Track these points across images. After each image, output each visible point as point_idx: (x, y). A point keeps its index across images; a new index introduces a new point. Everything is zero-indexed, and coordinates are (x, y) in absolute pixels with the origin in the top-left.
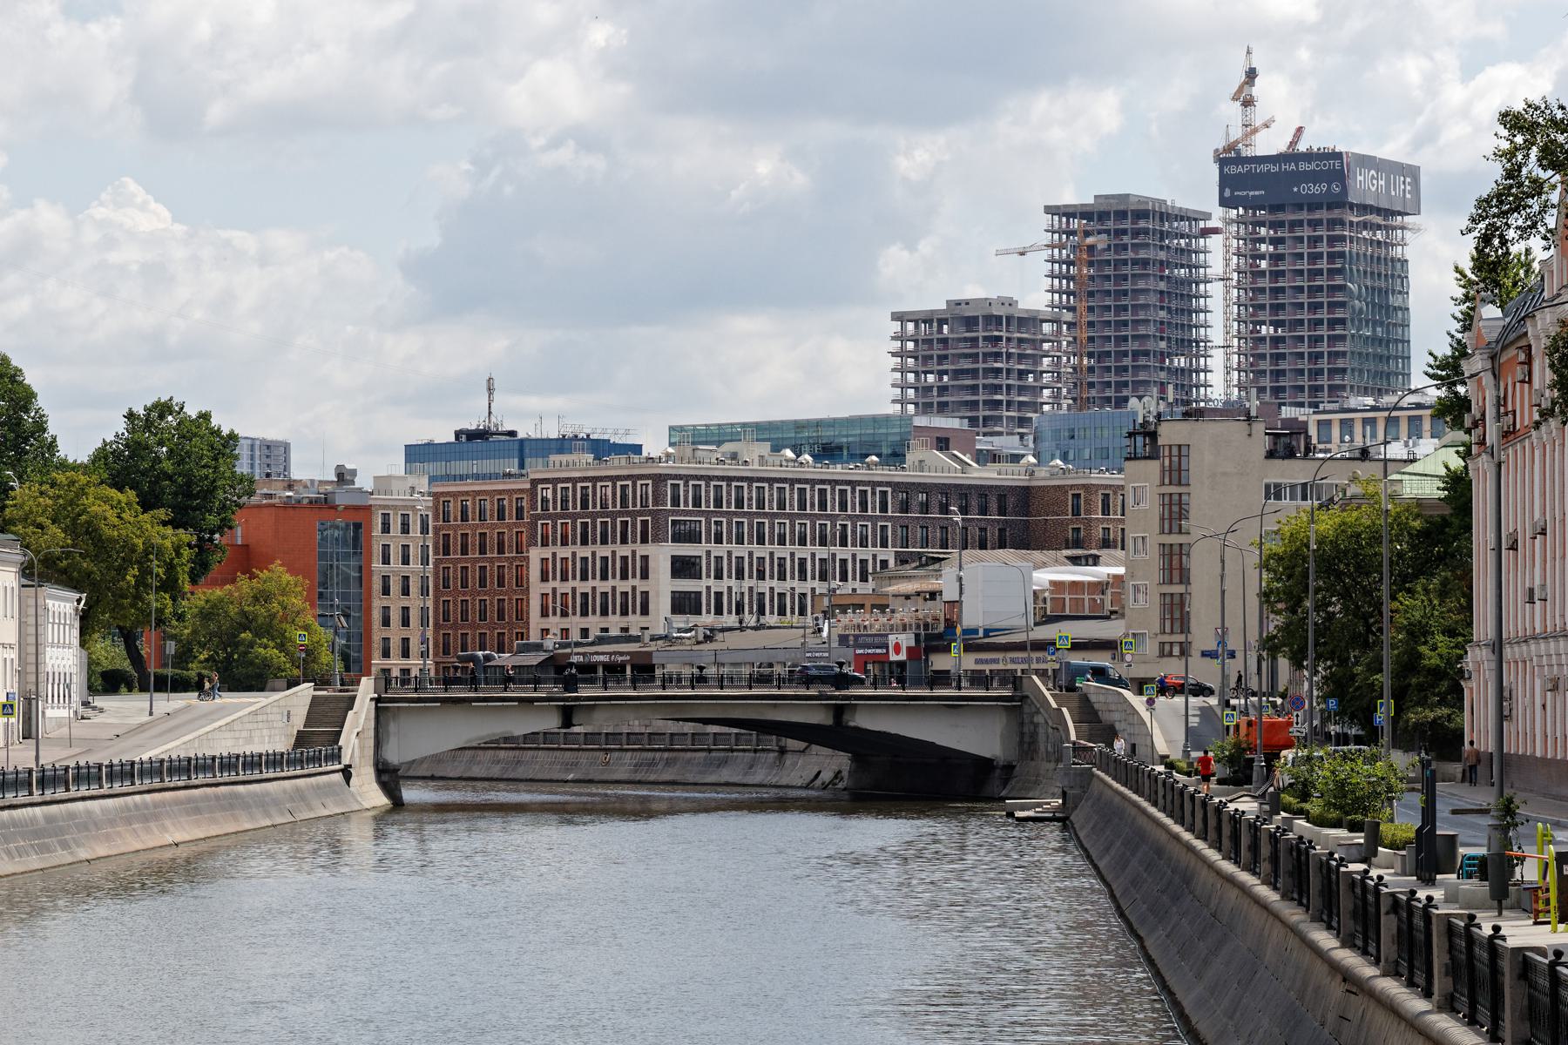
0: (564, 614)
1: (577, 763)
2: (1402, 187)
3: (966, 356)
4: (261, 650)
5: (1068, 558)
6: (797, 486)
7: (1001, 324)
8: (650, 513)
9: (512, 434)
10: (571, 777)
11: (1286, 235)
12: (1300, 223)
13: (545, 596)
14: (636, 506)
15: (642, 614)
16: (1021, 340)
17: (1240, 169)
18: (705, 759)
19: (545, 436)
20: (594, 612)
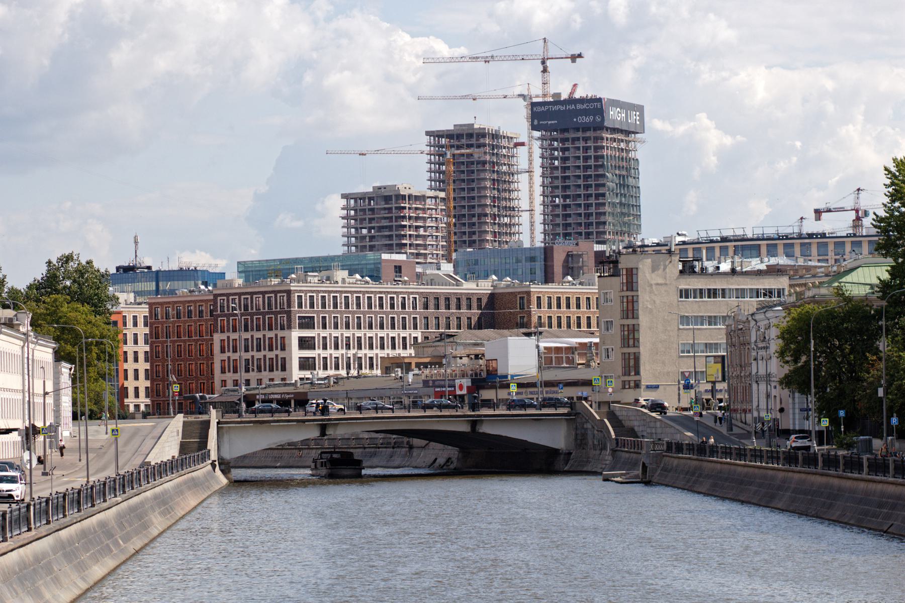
0: (235, 371)
1: (282, 457)
2: (634, 117)
3: (385, 218)
5: (523, 333)
6: (367, 295)
7: (405, 200)
8: (286, 312)
9: (149, 268)
10: (278, 464)
11: (570, 146)
12: (578, 139)
13: (223, 361)
15: (282, 370)
16: (417, 209)
17: (543, 109)
18: (362, 453)
19: (170, 269)
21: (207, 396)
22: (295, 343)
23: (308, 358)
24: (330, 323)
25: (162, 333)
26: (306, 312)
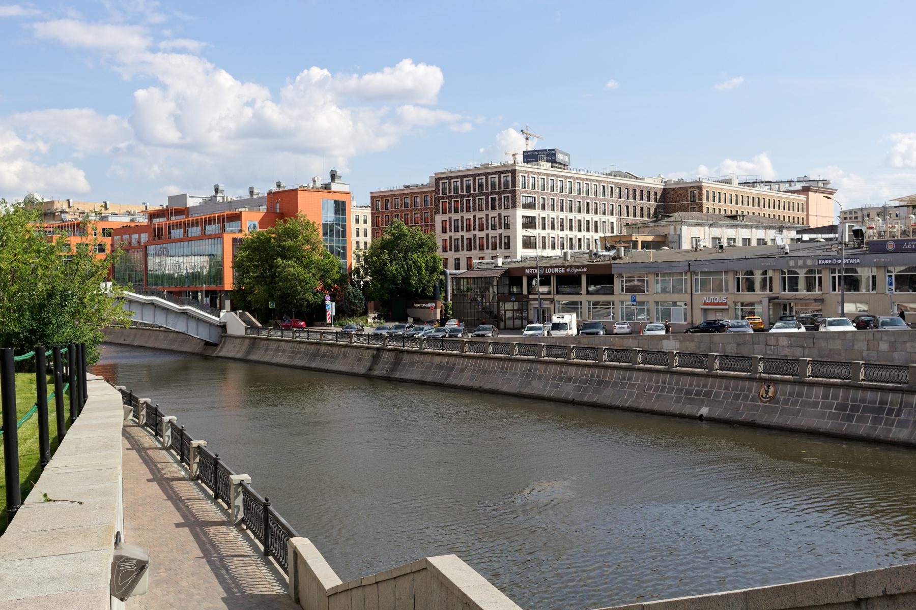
4: (291, 269)
8: (510, 192)
20: (475, 248)
22: (519, 222)
23: (530, 237)
25: (382, 221)
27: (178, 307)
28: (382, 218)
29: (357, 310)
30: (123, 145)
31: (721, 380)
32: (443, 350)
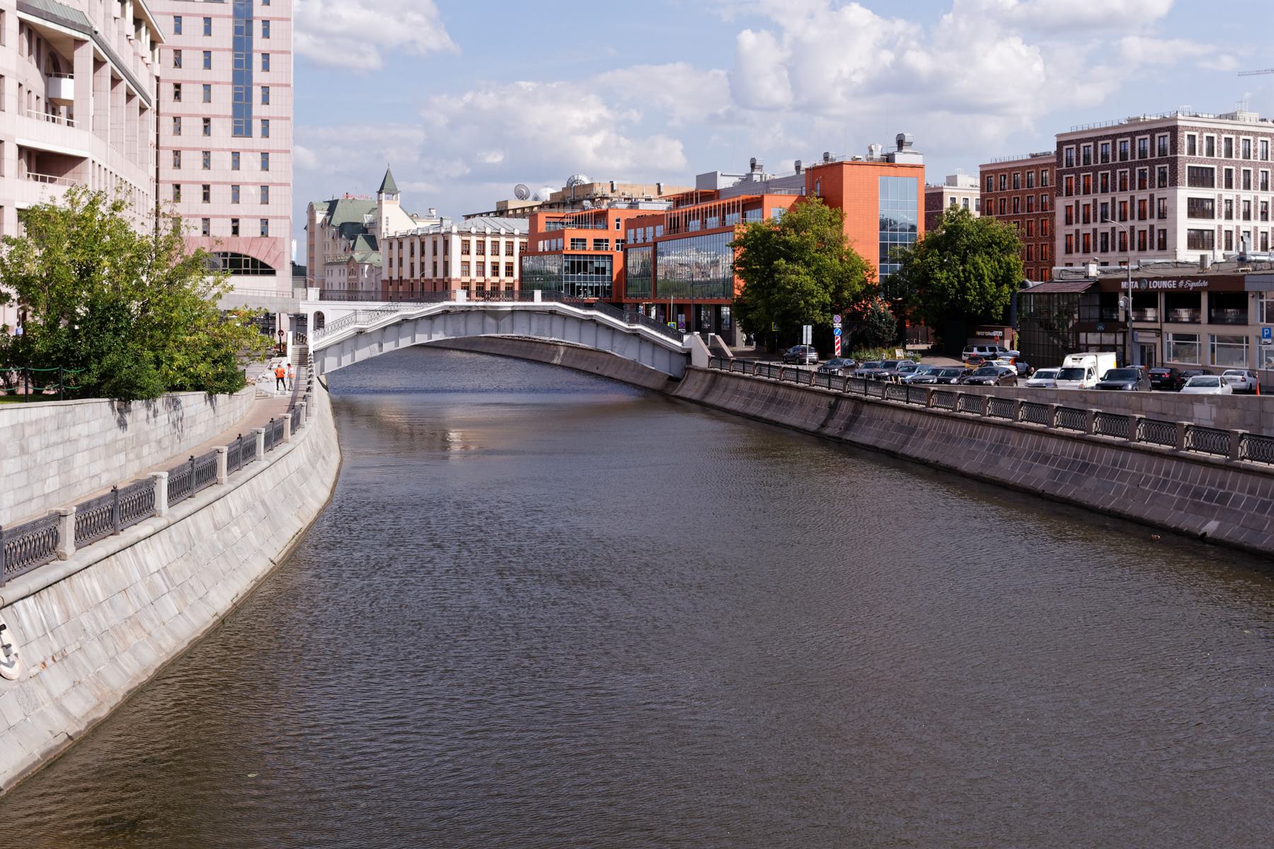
4: (794, 277)
8: (1168, 161)
13: (1068, 236)
14: (1154, 156)
20: (1113, 249)
21: (1031, 284)
22: (1182, 208)
23: (1202, 231)
24: (1238, 179)
26: (1202, 161)
27: (626, 326)
28: (996, 202)
29: (884, 338)
30: (721, 111)
31: (1246, 476)
32: (908, 403)
